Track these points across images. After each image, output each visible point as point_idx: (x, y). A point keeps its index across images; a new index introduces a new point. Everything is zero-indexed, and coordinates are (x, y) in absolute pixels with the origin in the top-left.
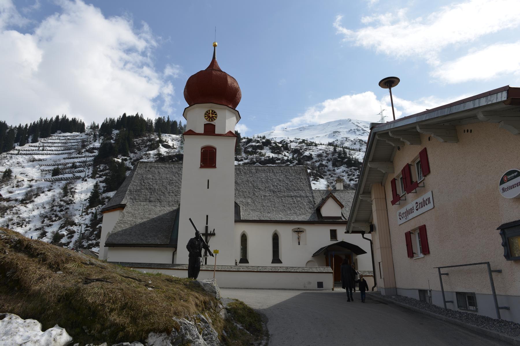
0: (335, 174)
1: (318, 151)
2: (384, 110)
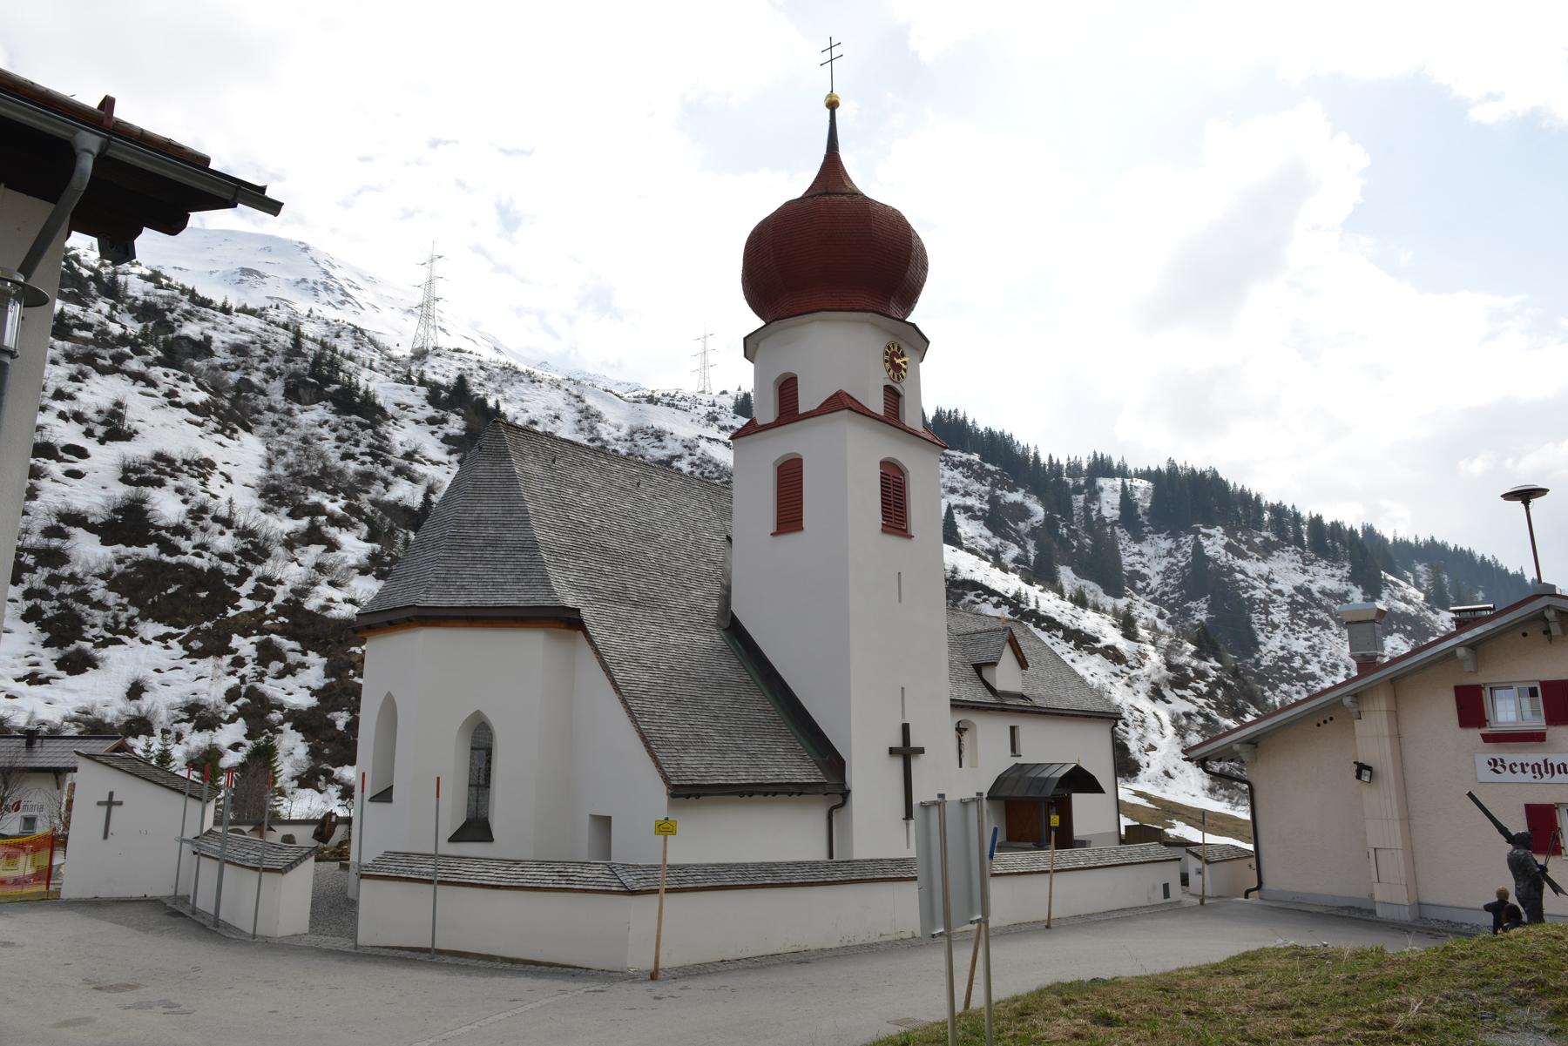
0: (293, 426)
1: (232, 332)
2: (440, 257)
